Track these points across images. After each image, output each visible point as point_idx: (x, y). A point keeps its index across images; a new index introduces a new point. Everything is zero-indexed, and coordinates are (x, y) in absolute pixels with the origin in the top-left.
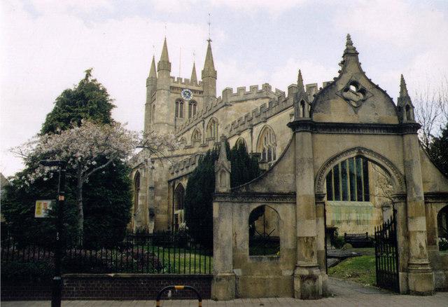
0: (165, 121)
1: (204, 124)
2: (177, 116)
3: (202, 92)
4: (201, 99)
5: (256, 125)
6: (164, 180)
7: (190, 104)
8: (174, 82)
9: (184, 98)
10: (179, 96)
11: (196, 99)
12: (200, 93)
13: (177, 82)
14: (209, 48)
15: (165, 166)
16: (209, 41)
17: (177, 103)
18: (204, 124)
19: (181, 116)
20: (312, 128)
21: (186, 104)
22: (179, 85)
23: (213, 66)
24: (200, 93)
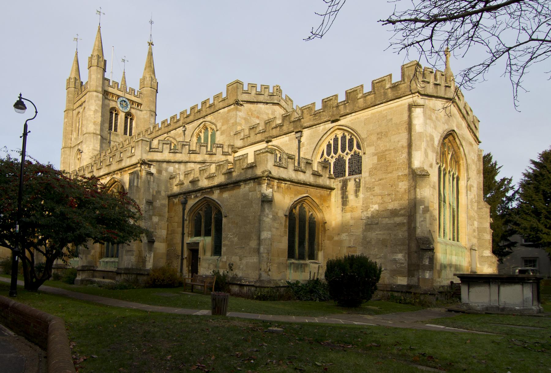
2: (110, 129)
7: (126, 118)
16: (151, 44)
19: (116, 130)
21: (122, 116)
24: (138, 106)
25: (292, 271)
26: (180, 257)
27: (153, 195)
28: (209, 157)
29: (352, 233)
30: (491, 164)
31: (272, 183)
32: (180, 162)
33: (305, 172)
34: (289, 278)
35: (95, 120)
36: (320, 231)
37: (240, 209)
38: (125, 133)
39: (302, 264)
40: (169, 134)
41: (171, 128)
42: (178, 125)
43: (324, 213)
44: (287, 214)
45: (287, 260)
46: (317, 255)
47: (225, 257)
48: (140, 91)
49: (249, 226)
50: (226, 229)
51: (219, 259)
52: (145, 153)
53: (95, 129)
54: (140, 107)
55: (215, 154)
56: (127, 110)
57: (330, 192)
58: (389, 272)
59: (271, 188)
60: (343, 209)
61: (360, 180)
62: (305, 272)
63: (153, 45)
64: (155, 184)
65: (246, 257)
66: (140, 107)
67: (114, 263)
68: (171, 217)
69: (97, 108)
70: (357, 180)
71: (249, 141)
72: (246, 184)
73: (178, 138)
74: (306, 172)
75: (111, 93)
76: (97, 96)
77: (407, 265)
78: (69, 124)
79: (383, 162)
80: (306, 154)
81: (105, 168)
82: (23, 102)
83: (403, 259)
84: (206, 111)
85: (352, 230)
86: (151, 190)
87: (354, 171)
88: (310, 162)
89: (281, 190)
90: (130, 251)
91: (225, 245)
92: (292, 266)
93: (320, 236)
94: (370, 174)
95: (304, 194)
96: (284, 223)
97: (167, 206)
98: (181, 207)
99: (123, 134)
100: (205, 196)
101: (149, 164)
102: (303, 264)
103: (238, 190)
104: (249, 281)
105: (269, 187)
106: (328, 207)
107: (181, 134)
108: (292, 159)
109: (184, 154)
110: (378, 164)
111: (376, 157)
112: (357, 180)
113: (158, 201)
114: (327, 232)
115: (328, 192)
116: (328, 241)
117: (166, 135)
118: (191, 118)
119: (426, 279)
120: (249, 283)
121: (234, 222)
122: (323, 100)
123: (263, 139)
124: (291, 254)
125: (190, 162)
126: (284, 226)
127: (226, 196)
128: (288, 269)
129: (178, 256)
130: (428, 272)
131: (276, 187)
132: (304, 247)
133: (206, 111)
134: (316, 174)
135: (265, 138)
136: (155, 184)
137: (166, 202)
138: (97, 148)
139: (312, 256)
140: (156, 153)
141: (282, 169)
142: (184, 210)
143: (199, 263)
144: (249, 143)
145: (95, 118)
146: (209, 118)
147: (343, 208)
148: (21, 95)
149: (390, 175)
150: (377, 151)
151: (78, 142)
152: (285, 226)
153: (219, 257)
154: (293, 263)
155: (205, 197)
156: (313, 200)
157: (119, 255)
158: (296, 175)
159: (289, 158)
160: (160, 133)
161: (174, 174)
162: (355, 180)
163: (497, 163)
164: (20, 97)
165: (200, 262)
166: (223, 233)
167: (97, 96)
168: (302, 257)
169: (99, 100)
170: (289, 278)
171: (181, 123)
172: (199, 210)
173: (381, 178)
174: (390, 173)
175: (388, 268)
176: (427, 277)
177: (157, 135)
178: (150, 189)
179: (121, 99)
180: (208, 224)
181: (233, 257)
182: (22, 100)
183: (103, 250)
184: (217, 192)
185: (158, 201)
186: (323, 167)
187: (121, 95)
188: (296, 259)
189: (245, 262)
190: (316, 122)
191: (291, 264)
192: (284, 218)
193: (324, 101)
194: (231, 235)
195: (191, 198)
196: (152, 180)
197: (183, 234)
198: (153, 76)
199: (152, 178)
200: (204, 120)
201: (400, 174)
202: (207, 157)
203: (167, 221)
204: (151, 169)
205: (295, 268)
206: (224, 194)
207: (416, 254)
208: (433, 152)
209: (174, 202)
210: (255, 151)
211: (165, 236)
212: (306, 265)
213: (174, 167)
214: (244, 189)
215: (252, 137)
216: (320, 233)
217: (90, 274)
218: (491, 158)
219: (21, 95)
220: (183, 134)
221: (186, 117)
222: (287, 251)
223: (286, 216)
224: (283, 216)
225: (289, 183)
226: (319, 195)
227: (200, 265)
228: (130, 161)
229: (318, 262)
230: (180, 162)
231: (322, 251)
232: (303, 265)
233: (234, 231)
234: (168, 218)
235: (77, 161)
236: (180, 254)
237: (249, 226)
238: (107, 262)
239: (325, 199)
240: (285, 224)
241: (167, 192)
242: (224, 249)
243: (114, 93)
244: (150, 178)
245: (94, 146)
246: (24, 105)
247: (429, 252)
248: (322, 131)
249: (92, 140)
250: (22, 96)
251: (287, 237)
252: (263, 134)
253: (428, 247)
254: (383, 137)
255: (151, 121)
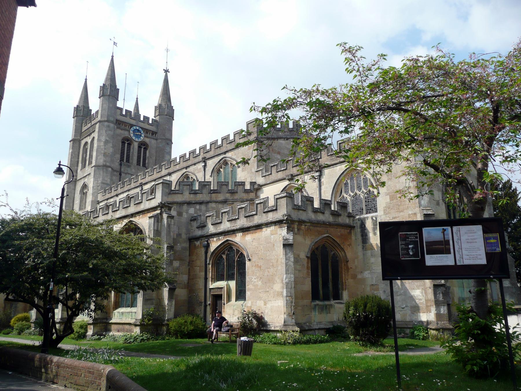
0: (108, 164)
1: (205, 167)
2: (122, 159)
3: (156, 133)
4: (153, 141)
5: (328, 166)
6: (184, 236)
7: (140, 147)
8: (122, 115)
9: (134, 138)
10: (125, 134)
11: (147, 140)
12: (153, 134)
13: (125, 116)
14: (166, 82)
15: (185, 215)
16: (166, 71)
17: (123, 143)
18: (205, 167)
19: (128, 161)
20: (23, 228)
21: (136, 145)
22: (127, 120)
23: (171, 103)
24: (153, 134)
25: (317, 313)
26: (203, 303)
27: (174, 239)
28: (231, 196)
29: (374, 271)
30: (512, 189)
31: (292, 226)
32: (201, 203)
33: (323, 213)
34: (314, 321)
35: (106, 151)
36: (343, 270)
37: (262, 252)
38: (138, 163)
39: (326, 306)
40: (188, 170)
41: (189, 163)
42: (197, 160)
43: (346, 251)
44: (309, 255)
45: (311, 302)
46: (342, 294)
47: (250, 302)
48: (154, 118)
49: (272, 269)
50: (250, 273)
51: (244, 304)
52: (166, 196)
53: (105, 161)
54: (154, 135)
55: (237, 192)
56: (141, 139)
57: (351, 230)
58: (409, 308)
59: (291, 231)
60: (363, 247)
61: (376, 218)
62: (330, 313)
63: (169, 72)
64: (175, 226)
65: (270, 301)
66: (154, 135)
67: (131, 314)
68: (193, 261)
69: (108, 139)
70: (374, 218)
71: (270, 178)
72: (267, 227)
73: (198, 173)
74: (325, 212)
75: (123, 122)
76: (109, 126)
77: (425, 301)
78: (75, 154)
79: (395, 201)
80: (326, 192)
81: (122, 210)
82: (62, 168)
83: (421, 295)
84: (227, 147)
85: (373, 268)
86: (172, 234)
87: (371, 209)
88: (329, 203)
89: (301, 232)
90: (152, 299)
91: (249, 290)
92: (317, 308)
93: (344, 275)
94: (384, 212)
95: (325, 234)
96: (306, 265)
97: (188, 248)
98: (203, 250)
99: (136, 165)
100: (228, 239)
101: (169, 207)
102: (328, 305)
103: (261, 233)
104: (274, 326)
105: (289, 230)
106: (349, 245)
107: (200, 169)
108: (310, 201)
109: (205, 195)
110: (391, 203)
111: (388, 197)
112: (374, 218)
113: (178, 244)
114: (350, 270)
115: (349, 231)
116: (352, 280)
117: (184, 170)
118: (211, 154)
119: (441, 314)
120: (274, 328)
121: (258, 265)
122: (338, 141)
123: (285, 177)
124: (315, 296)
125: (211, 202)
126: (306, 267)
127: (248, 238)
128: (312, 311)
129: (202, 302)
130: (442, 307)
131: (296, 230)
132: (328, 287)
133: (227, 147)
134: (334, 214)
135: (286, 176)
136: (175, 226)
137: (186, 245)
138: (106, 181)
139: (337, 296)
140: (177, 195)
141: (301, 212)
142: (206, 253)
143: (223, 310)
144: (271, 180)
145: (105, 149)
146: (229, 155)
147: (363, 246)
148: (60, 162)
149: (402, 214)
150: (389, 191)
151: (85, 175)
152: (307, 268)
153: (243, 302)
154: (318, 305)
155: (227, 240)
156: (334, 240)
157: (138, 305)
158: (315, 216)
159: (307, 200)
160: (178, 167)
161: (195, 215)
162: (372, 218)
163: (517, 189)
164: (60, 165)
165: (224, 308)
166: (247, 277)
167: (109, 126)
168: (326, 298)
169: (110, 130)
170: (314, 321)
171: (200, 158)
172: (222, 254)
173: (394, 216)
174: (402, 211)
175: (409, 305)
176: (442, 312)
177: (175, 170)
178: (170, 233)
179: (135, 128)
180: (230, 266)
181: (258, 302)
182: (61, 166)
183: (117, 299)
184: (239, 235)
185: (178, 244)
186: (342, 206)
187: (135, 124)
188: (321, 301)
189: (270, 307)
190: (333, 163)
191: (315, 305)
192: (306, 259)
193: (339, 142)
194: (255, 279)
195: (213, 241)
196: (172, 223)
197: (206, 279)
198: (169, 103)
199: (172, 221)
200: (224, 156)
201: (410, 213)
202: (228, 196)
203: (189, 265)
204: (172, 211)
205: (320, 310)
206: (246, 237)
207: (430, 290)
208: (438, 190)
209: (195, 245)
210: (275, 196)
211: (186, 282)
212: (331, 305)
213: (195, 208)
214: (266, 232)
215: (273, 174)
216: (343, 272)
217: (103, 327)
218: (511, 184)
219: (60, 162)
220: (203, 169)
221: (206, 153)
222: (311, 292)
223: (307, 257)
224: (305, 257)
225: (309, 224)
226: (339, 234)
227: (224, 311)
228: (149, 204)
229: (342, 302)
230: (201, 203)
231: (347, 290)
232: (328, 306)
233: (258, 275)
234: (189, 263)
235: (83, 195)
236: (203, 301)
237: (272, 269)
238: (122, 313)
239: (346, 238)
240: (307, 265)
241: (188, 235)
242: (248, 294)
243: (126, 122)
244: (171, 221)
245: (103, 179)
246: (63, 171)
247: (441, 288)
248: (339, 171)
249: (101, 173)
250: (61, 163)
251: (310, 278)
252: (284, 172)
253: (440, 282)
254: (393, 178)
255: (167, 150)
